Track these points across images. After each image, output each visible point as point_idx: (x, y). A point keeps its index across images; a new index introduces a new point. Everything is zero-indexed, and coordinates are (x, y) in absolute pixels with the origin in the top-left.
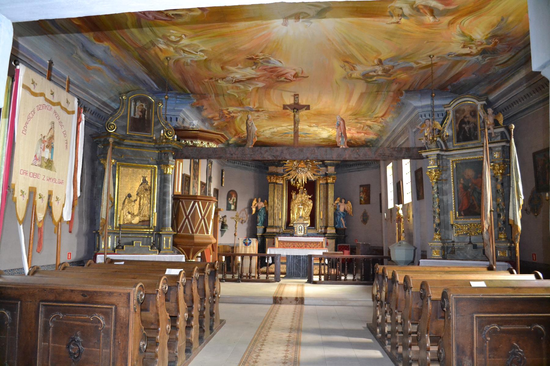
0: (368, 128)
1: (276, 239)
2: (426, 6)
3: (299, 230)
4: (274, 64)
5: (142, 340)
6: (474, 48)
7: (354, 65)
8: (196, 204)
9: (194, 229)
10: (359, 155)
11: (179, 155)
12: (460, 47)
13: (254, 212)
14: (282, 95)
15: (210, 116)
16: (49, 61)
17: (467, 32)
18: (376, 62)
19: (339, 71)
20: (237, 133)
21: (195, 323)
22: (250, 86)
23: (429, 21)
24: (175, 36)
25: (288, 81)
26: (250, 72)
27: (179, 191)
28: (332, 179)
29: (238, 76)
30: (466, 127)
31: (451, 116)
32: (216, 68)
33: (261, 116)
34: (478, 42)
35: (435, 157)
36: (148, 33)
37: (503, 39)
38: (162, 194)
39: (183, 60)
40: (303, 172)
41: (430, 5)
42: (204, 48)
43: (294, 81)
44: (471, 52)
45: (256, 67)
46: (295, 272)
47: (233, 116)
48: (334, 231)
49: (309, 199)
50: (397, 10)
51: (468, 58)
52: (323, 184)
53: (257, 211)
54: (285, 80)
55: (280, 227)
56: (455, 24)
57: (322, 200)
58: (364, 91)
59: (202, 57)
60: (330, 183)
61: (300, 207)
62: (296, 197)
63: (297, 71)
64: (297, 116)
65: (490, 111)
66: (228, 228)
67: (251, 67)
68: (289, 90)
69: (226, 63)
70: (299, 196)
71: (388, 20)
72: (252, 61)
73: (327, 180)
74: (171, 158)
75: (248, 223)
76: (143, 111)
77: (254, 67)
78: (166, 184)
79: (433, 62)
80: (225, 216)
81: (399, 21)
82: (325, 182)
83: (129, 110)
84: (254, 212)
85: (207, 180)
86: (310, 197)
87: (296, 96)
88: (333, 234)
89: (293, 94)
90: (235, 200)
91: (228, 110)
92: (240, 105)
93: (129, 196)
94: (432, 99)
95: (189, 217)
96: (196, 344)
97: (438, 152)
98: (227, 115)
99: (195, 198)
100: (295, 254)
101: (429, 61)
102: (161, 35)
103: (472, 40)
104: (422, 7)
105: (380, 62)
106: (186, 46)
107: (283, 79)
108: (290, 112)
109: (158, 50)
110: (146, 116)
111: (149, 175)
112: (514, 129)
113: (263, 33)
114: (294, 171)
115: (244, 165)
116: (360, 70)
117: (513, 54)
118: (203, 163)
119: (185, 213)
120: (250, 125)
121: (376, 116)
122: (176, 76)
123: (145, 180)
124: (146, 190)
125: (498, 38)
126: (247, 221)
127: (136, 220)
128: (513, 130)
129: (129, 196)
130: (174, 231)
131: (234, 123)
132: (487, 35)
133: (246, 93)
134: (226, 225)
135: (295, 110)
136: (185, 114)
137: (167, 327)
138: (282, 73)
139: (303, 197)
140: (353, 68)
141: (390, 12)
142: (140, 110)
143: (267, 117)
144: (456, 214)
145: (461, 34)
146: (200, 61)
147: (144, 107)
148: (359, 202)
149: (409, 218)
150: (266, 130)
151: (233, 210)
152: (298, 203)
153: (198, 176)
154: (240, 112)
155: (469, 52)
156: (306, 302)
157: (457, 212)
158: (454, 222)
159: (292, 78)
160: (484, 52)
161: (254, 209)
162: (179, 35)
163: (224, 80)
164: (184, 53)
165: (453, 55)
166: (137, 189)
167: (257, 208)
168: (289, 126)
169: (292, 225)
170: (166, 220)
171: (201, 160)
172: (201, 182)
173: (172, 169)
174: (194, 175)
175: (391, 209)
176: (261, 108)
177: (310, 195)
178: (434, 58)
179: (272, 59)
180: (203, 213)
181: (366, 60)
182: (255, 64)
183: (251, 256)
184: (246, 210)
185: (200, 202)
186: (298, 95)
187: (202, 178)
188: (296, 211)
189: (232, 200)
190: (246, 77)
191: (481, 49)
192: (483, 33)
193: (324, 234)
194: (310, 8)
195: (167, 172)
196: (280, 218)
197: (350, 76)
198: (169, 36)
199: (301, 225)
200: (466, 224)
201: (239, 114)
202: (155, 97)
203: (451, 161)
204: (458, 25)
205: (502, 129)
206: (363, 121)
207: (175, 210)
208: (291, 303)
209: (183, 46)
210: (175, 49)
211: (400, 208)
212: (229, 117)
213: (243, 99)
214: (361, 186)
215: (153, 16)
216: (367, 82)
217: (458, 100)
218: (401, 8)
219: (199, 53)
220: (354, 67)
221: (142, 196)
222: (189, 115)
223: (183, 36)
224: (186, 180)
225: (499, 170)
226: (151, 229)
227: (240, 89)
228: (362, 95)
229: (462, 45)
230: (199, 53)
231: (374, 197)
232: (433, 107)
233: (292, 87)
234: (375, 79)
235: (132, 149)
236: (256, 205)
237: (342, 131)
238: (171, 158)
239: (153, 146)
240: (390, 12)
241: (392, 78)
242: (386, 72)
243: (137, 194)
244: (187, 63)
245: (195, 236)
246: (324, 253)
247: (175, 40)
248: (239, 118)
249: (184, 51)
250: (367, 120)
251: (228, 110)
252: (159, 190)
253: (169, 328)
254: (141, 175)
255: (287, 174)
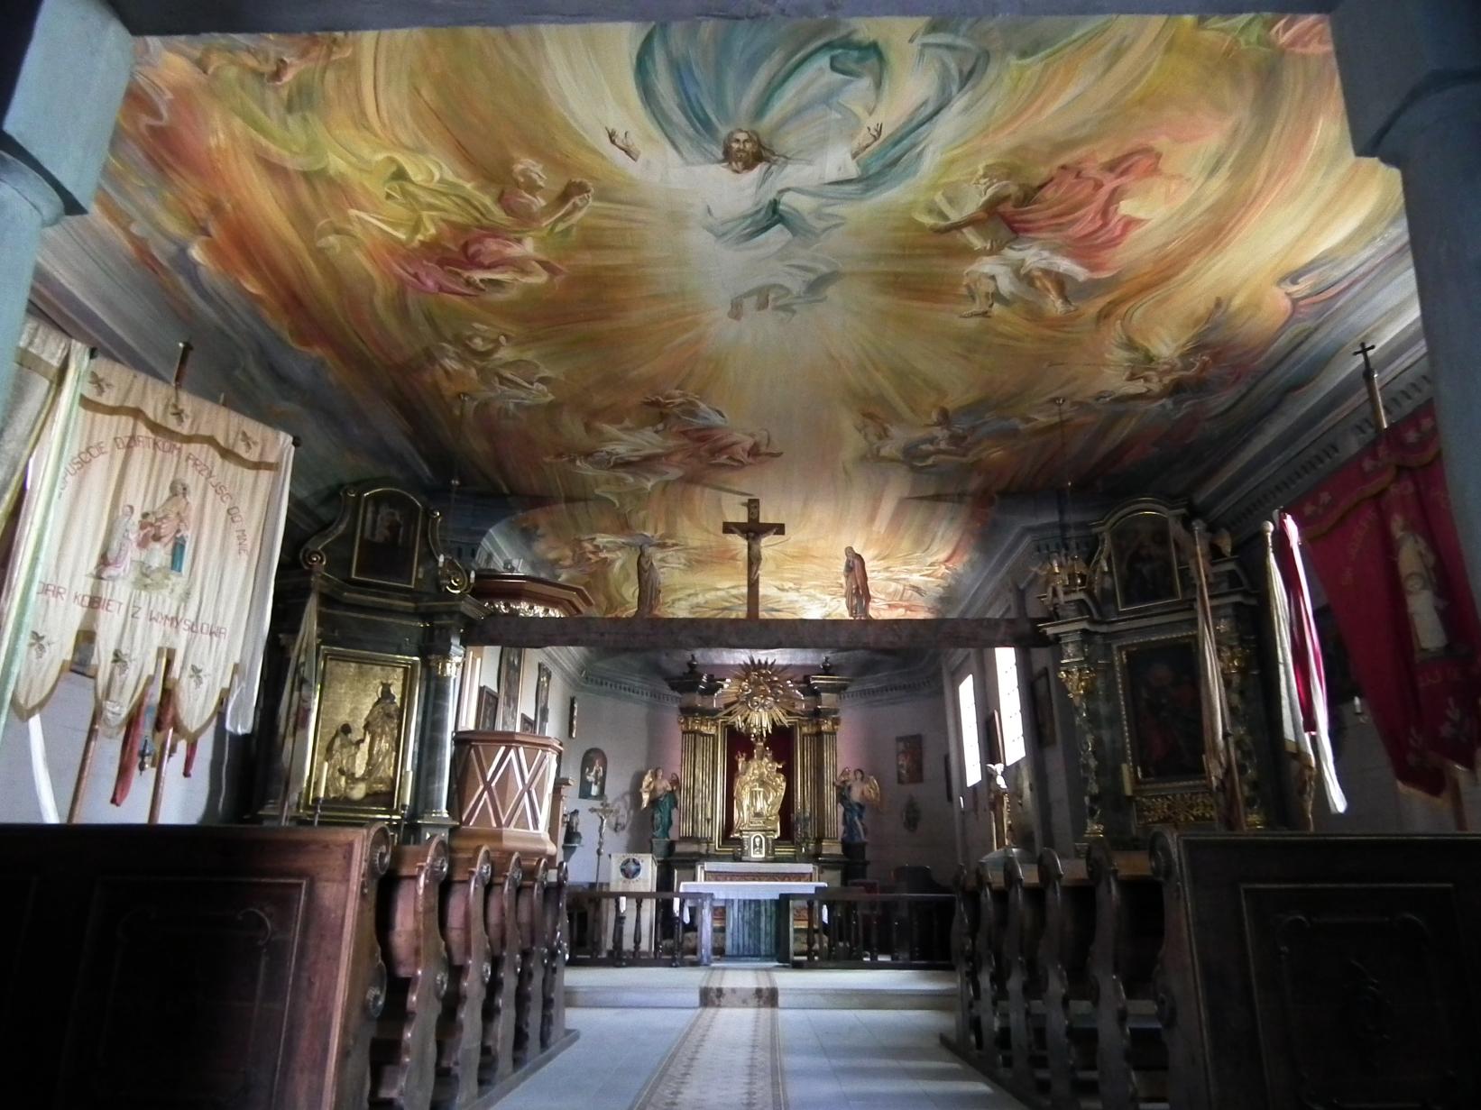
0: (916, 594)
1: (699, 867)
2: (1047, 273)
3: (755, 846)
4: (706, 418)
5: (373, 984)
6: (1156, 379)
7: (887, 425)
8: (512, 754)
9: (504, 815)
10: (900, 638)
11: (475, 636)
12: (1124, 378)
13: (645, 805)
14: (719, 500)
15: (552, 555)
16: (184, 343)
17: (1139, 340)
18: (934, 416)
19: (853, 441)
20: (612, 605)
21: (505, 1002)
22: (648, 476)
23: (1054, 310)
24: (484, 339)
25: (736, 464)
26: (648, 440)
27: (468, 723)
28: (830, 723)
29: (621, 449)
30: (1146, 569)
31: (1107, 545)
32: (573, 428)
33: (670, 559)
34: (1165, 363)
35: (1077, 638)
36: (420, 328)
37: (1219, 353)
38: (428, 726)
39: (498, 404)
40: (763, 706)
41: (1056, 269)
42: (546, 373)
43: (751, 464)
44: (1149, 390)
45: (665, 426)
46: (746, 943)
47: (606, 558)
48: (837, 849)
49: (778, 770)
50: (985, 281)
51: (1142, 406)
52: (810, 735)
53: (654, 802)
54: (729, 462)
55: (709, 841)
56: (1112, 318)
57: (809, 774)
58: (906, 495)
59: (542, 394)
60: (827, 733)
61: (757, 789)
62: (747, 768)
63: (757, 438)
64: (755, 547)
65: (1198, 526)
66: (583, 841)
67: (653, 425)
68: (736, 489)
69: (595, 414)
70: (754, 764)
71: (962, 308)
72: (656, 410)
73: (818, 725)
74: (455, 641)
75: (631, 830)
76: (393, 528)
77: (660, 426)
78: (440, 702)
79: (1065, 417)
80: (576, 812)
81: (987, 309)
82: (814, 730)
83: (361, 517)
84: (645, 805)
85: (536, 715)
86: (780, 767)
87: (753, 505)
88: (836, 855)
89: (745, 499)
90: (601, 774)
91: (595, 543)
92: (623, 529)
93: (346, 729)
94: (1061, 512)
95: (493, 784)
96: (505, 1062)
97: (1084, 625)
98: (591, 556)
99: (508, 740)
100: (747, 897)
101: (1055, 415)
102: (449, 335)
103: (1149, 359)
104: (1039, 274)
105: (945, 418)
106: (507, 365)
107: (723, 459)
108: (739, 543)
109: (440, 372)
110: (400, 540)
111: (397, 680)
112: (1274, 533)
113: (686, 336)
114: (742, 703)
115: (625, 689)
116: (899, 437)
117: (1244, 390)
118: (533, 657)
119: (484, 777)
120: (646, 567)
121: (934, 559)
122: (478, 445)
123: (389, 691)
124: (389, 716)
125: (1208, 351)
126: (627, 828)
127: (359, 792)
128: (1269, 534)
129: (346, 729)
130: (454, 819)
131: (605, 578)
132: (1184, 346)
133: (639, 496)
134: (578, 835)
135: (752, 534)
136: (493, 543)
137: (438, 978)
138: (724, 442)
139: (761, 767)
140: (884, 435)
141: (968, 286)
142: (387, 524)
143: (683, 561)
144: (1136, 772)
145: (1126, 344)
146: (538, 406)
147: (398, 518)
148: (896, 777)
149: (1021, 797)
150: (679, 599)
151: (596, 798)
152: (753, 781)
153: (515, 700)
154: (621, 547)
155: (1144, 390)
156: (781, 1000)
157: (1139, 769)
158: (1134, 791)
159: (744, 457)
160: (1177, 389)
161: (646, 797)
162: (495, 336)
163: (590, 459)
164: (501, 383)
165: (1108, 399)
166: (367, 713)
167: (653, 792)
168: (733, 587)
169: (737, 835)
170: (433, 790)
171: (528, 650)
172: (523, 715)
173: (458, 665)
174: (507, 694)
175: (974, 787)
176: (670, 537)
177: (779, 763)
178: (1066, 407)
179: (703, 406)
180: (527, 777)
181: (913, 410)
182: (663, 417)
183: (639, 898)
184: (628, 798)
185: (521, 750)
186: (757, 501)
187: (527, 707)
188: (746, 802)
189: (593, 774)
190: (642, 453)
191: (1172, 380)
192: (1175, 341)
193: (813, 858)
194: (790, 274)
195: (443, 673)
196: (709, 816)
197: (875, 452)
198: (470, 338)
199: (759, 834)
200: (1162, 797)
201: (619, 554)
202: (424, 498)
203: (1114, 646)
204: (1119, 322)
205: (1230, 566)
206: (903, 576)
207: (459, 771)
208: (745, 1003)
209: (501, 366)
210: (480, 371)
211: (999, 773)
212: (597, 562)
213: (630, 512)
214: (899, 739)
215: (437, 283)
216: (913, 469)
217: (1113, 515)
218: (993, 278)
219: (536, 384)
220: (885, 430)
221: (379, 730)
222: (503, 547)
223: (502, 339)
224: (488, 701)
225: (1232, 660)
226: (396, 813)
227: (625, 484)
228: (903, 502)
229: (1127, 373)
230: (536, 384)
231: (931, 765)
232: (1063, 527)
233: (746, 482)
234: (930, 461)
235: (362, 616)
236: (652, 786)
237: (859, 581)
238: (455, 641)
239: (412, 611)
240: (968, 286)
241: (970, 458)
242: (956, 439)
243: (366, 727)
244: (507, 411)
245: (504, 833)
246: (817, 889)
247: (483, 350)
248: (618, 564)
249: (503, 380)
250: (909, 572)
251: (595, 543)
252: (420, 719)
253: (442, 983)
254: (378, 681)
255: (725, 712)
